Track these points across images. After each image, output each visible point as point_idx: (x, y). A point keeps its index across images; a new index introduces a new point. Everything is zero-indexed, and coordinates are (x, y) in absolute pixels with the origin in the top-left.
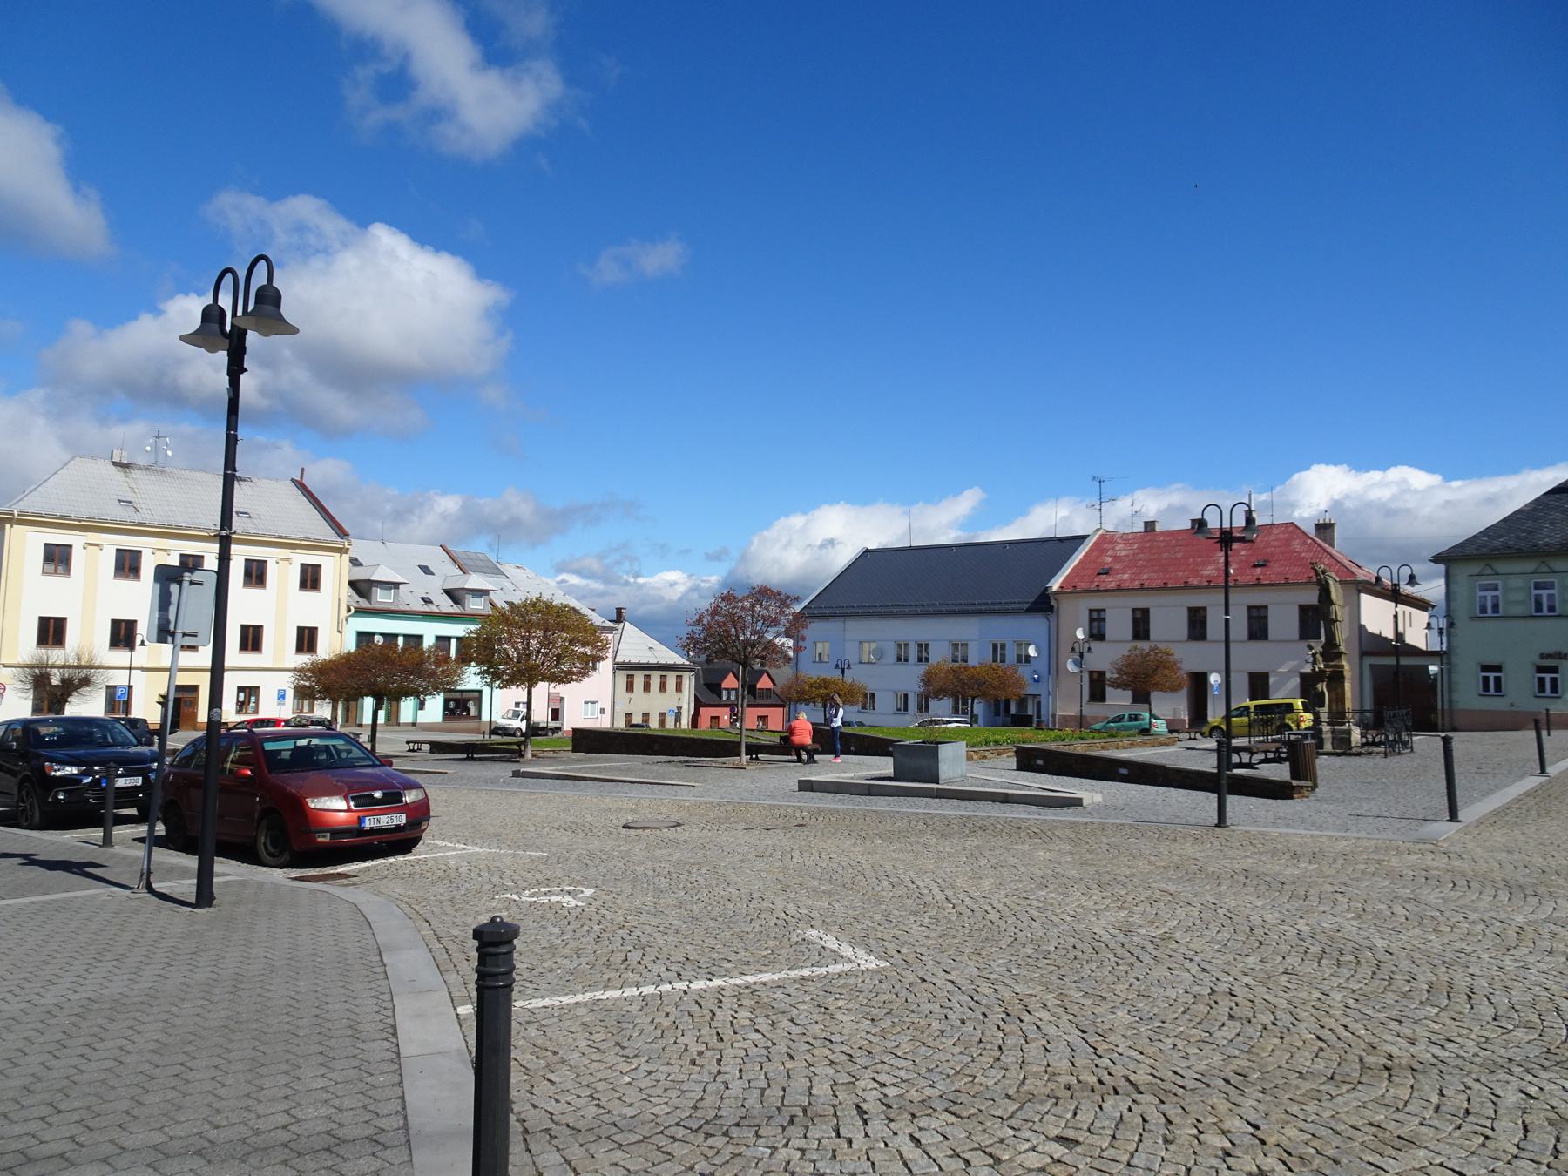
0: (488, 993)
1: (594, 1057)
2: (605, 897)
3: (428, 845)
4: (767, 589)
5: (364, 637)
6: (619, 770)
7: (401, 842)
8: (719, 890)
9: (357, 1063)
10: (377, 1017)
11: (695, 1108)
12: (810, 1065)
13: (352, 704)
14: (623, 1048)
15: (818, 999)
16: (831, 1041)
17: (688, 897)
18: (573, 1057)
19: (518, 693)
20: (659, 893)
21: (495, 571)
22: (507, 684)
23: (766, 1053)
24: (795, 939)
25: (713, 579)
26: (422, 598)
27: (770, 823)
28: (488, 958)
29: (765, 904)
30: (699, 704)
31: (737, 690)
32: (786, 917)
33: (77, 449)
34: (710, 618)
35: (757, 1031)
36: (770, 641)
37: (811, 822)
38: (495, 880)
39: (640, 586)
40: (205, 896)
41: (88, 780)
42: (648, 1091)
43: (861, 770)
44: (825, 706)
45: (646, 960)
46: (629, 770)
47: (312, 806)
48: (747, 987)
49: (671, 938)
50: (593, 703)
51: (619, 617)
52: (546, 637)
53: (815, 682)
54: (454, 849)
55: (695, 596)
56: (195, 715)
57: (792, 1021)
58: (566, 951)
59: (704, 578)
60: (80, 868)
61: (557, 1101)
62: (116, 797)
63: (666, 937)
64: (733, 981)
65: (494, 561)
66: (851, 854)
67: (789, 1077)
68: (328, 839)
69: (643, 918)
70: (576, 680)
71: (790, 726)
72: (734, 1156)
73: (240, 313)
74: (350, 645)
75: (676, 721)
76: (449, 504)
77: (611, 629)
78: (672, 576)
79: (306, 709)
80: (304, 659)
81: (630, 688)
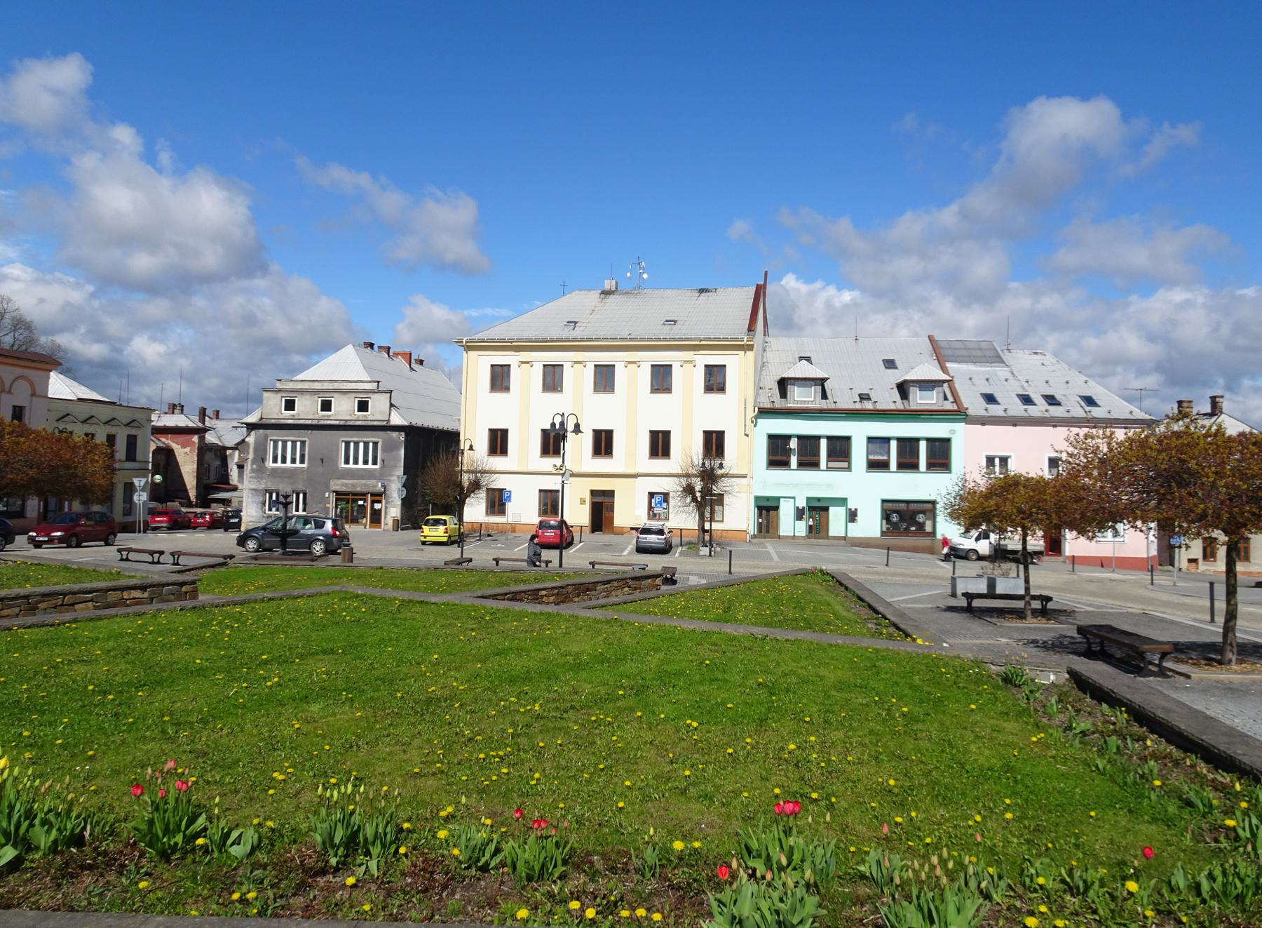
21: (998, 360)
46: (1174, 615)
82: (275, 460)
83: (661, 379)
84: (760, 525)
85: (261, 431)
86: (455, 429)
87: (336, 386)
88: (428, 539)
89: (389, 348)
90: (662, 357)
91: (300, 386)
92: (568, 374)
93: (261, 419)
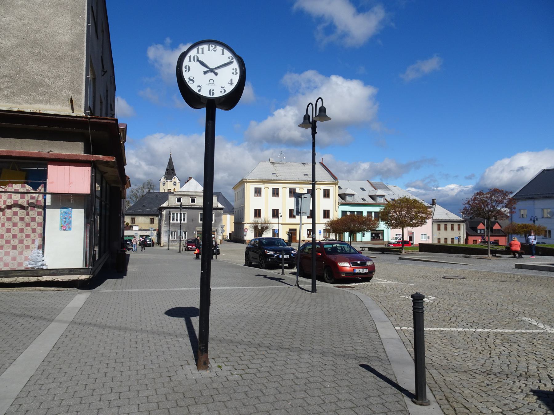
0: (417, 313)
1: (443, 346)
2: (439, 300)
3: (375, 280)
4: (497, 189)
5: (344, 213)
6: (438, 258)
7: (366, 278)
8: (484, 301)
9: (368, 338)
10: (371, 327)
11: (482, 366)
12: (527, 360)
13: (341, 235)
14: (454, 345)
15: (529, 340)
16: (536, 354)
17: (471, 302)
18: (436, 345)
19: (399, 231)
20: (460, 300)
22: (395, 227)
23: (509, 354)
24: (517, 320)
25: (470, 186)
26: (362, 199)
27: (503, 279)
28: (416, 304)
29: (503, 307)
30: (468, 235)
31: (484, 230)
32: (513, 312)
33: (258, 160)
34: (472, 202)
35: (505, 347)
36: (499, 210)
37: (522, 280)
38: (399, 291)
39: (439, 191)
40: (314, 289)
41: (276, 256)
42: (464, 359)
43: (545, 261)
44: (526, 236)
45: (458, 321)
47: (340, 265)
48: (499, 333)
49: (467, 315)
50: (425, 234)
51: (433, 203)
52: (408, 211)
53: (521, 226)
54: (383, 281)
55: (463, 193)
56: (296, 238)
57: (518, 345)
58: (428, 315)
59: (466, 186)
60: (279, 280)
61: (433, 357)
62: (285, 261)
63: (464, 314)
64: (493, 331)
65: (386, 185)
66: (541, 293)
67: (519, 362)
68: (344, 275)
69: (455, 307)
70: (420, 226)
71: (510, 243)
72: (499, 381)
73: (314, 116)
74: (340, 216)
75: (458, 241)
76: (365, 166)
77: (431, 207)
78: (452, 186)
79: (327, 236)
80: (327, 220)
81: (439, 229)
82: (173, 220)
83: (276, 193)
85: (168, 210)
87: (197, 194)
92: (263, 191)
93: (168, 205)
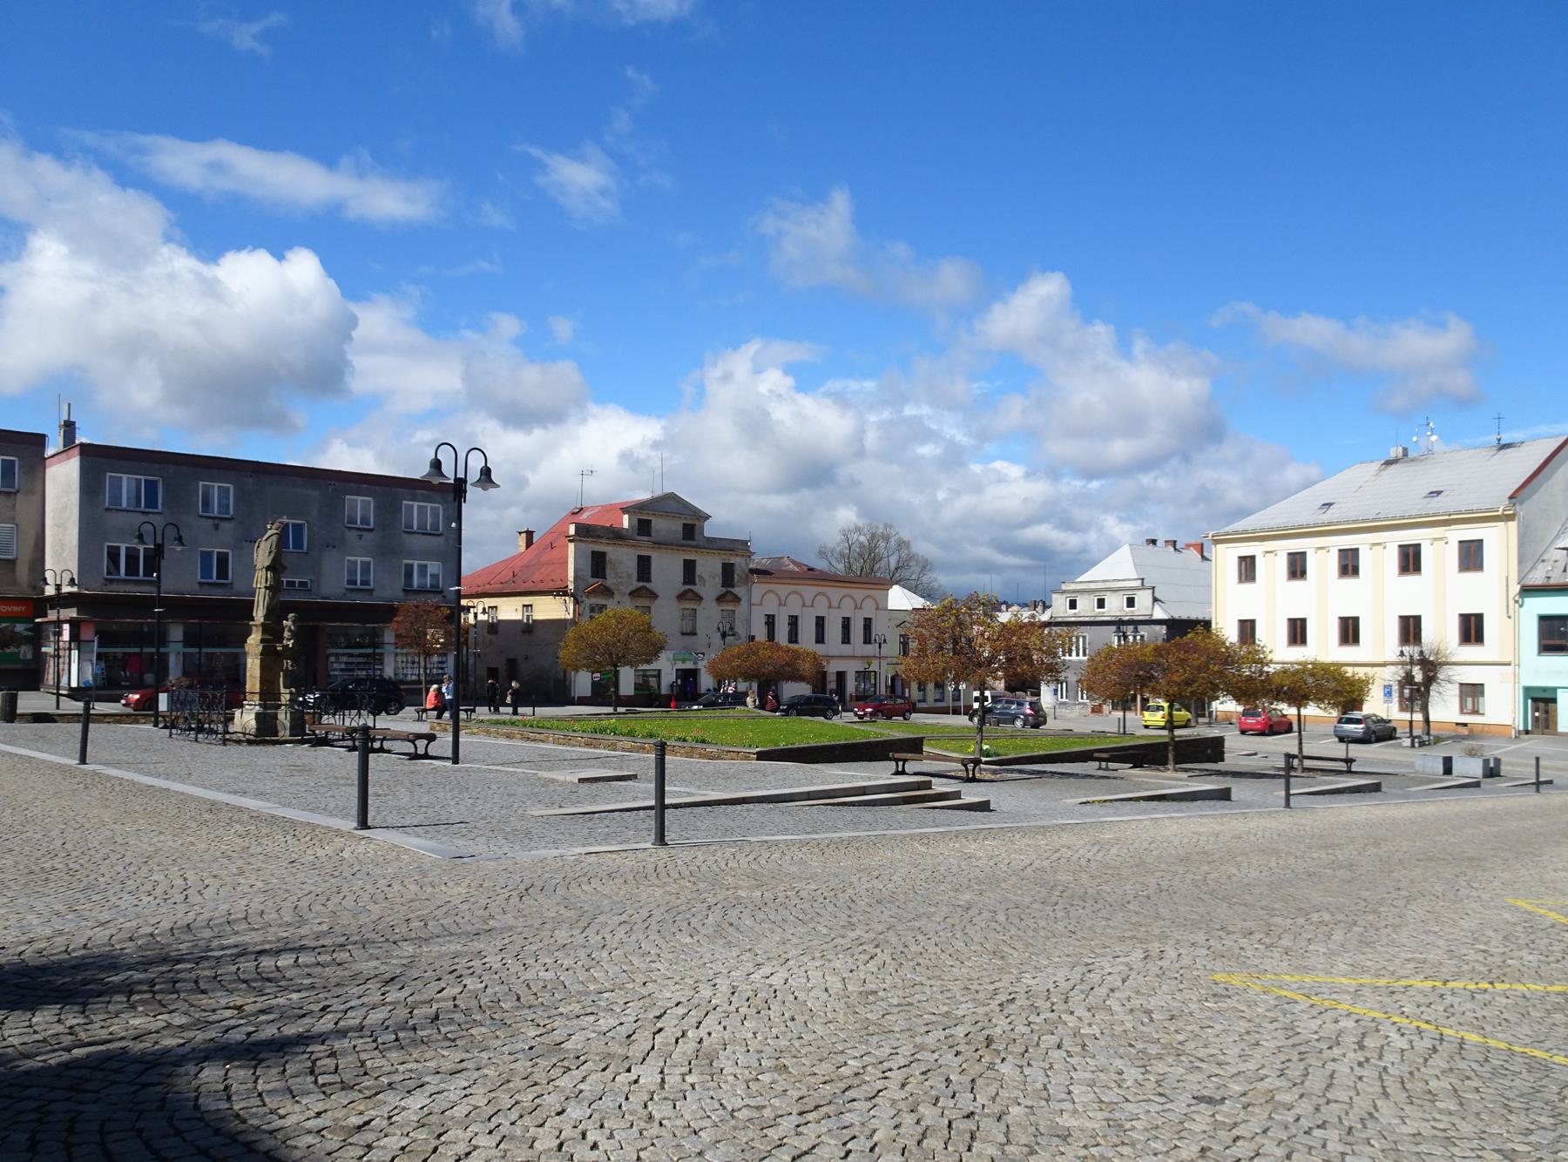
84: (1536, 720)
86: (1207, 619)
87: (1108, 585)
88: (1148, 723)
89: (1175, 542)
90: (1409, 537)
91: (1080, 587)
